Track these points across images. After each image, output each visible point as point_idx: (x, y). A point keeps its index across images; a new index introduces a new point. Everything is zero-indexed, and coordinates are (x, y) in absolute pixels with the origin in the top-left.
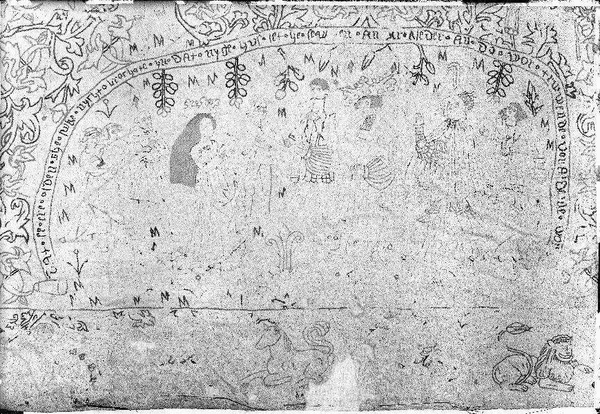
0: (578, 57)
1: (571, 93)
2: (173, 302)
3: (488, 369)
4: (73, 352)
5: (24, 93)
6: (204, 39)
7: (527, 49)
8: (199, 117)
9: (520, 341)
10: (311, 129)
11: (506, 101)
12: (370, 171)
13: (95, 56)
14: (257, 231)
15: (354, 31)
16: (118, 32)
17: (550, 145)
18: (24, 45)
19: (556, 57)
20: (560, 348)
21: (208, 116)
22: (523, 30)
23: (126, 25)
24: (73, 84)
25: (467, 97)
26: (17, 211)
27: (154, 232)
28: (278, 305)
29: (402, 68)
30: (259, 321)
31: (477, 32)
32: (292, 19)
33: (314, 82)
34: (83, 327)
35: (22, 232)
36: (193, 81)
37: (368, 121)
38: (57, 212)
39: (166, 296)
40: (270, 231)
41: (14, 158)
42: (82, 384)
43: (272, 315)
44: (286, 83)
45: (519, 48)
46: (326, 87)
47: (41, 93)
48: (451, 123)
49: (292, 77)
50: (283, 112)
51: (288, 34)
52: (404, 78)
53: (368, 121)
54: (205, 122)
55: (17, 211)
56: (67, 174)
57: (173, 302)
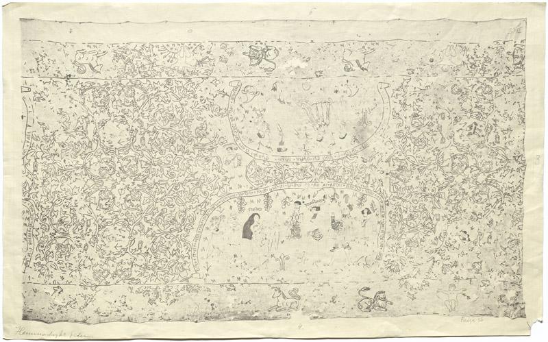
0: (390, 191)
1: (455, 200)
2: (242, 281)
3: (356, 304)
4: (205, 299)
5: (190, 204)
6: (256, 187)
7: (372, 189)
8: (253, 215)
9: (367, 294)
10: (294, 219)
11: (363, 208)
12: (316, 234)
13: (216, 191)
14: (272, 256)
15: (310, 184)
16: (225, 183)
17: (379, 223)
18: (191, 186)
19: (382, 191)
20: (381, 296)
21: (257, 214)
22: (371, 182)
23: (228, 180)
24: (208, 201)
25: (350, 207)
26: (186, 247)
27: (235, 256)
28: (279, 282)
29: (327, 197)
30: (273, 288)
31: (355, 183)
32: (289, 180)
33: (296, 202)
34: (209, 290)
35: (187, 255)
36: (252, 201)
37: (315, 216)
38: (201, 247)
39: (239, 279)
40: (277, 256)
41: (186, 227)
42: (209, 311)
43: (277, 286)
44: (285, 203)
45: (123, 288)
46: (300, 204)
47: (197, 204)
48: (344, 216)
49: (288, 200)
50: (284, 213)
51: (198, 90)
52: (328, 200)
53: (315, 216)
54: (256, 216)
55: (186, 247)
56: (205, 233)
57: (242, 281)
